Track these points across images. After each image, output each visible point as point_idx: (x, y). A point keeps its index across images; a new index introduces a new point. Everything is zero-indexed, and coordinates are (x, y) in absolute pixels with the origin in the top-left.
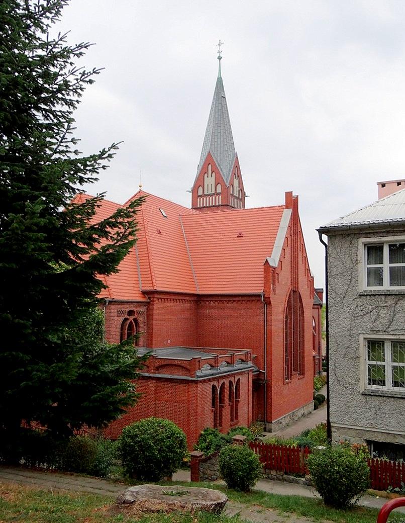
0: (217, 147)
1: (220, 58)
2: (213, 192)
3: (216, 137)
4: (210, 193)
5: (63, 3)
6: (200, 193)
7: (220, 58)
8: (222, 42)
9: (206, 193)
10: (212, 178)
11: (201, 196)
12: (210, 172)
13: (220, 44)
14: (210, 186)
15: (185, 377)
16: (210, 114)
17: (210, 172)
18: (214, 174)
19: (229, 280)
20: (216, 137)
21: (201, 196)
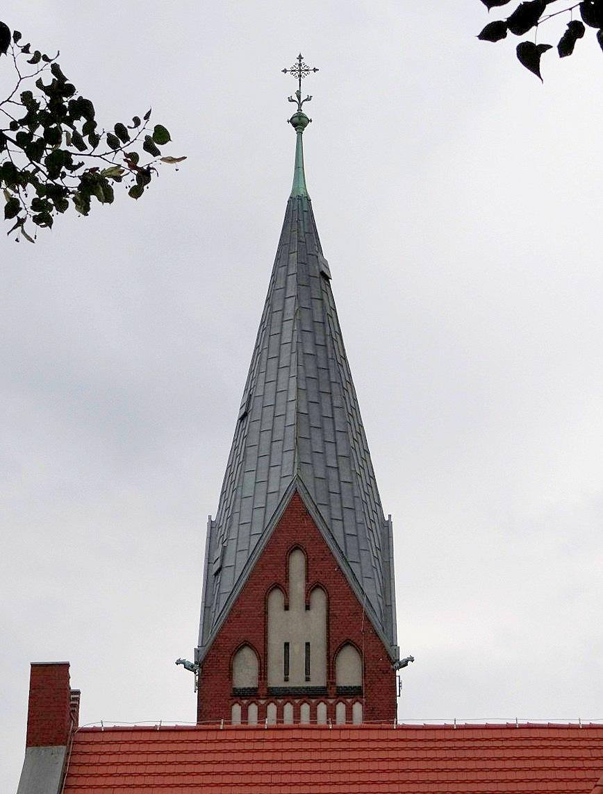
0: (326, 479)
1: (299, 122)
2: (335, 405)
3: (316, 436)
4: (297, 680)
5: (64, 188)
6: (245, 673)
7: (299, 122)
8: (308, 62)
9: (276, 679)
10: (311, 612)
11: (249, 695)
12: (298, 585)
13: (300, 70)
14: (297, 652)
15: (319, 525)
16: (222, 493)
17: (298, 585)
18: (319, 599)
19: (536, 753)
20: (316, 436)
21: (249, 695)
